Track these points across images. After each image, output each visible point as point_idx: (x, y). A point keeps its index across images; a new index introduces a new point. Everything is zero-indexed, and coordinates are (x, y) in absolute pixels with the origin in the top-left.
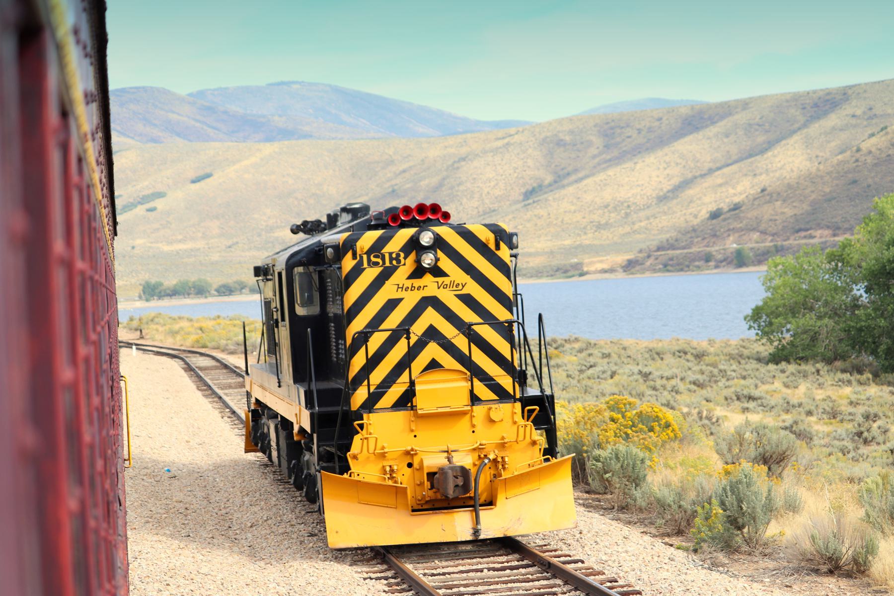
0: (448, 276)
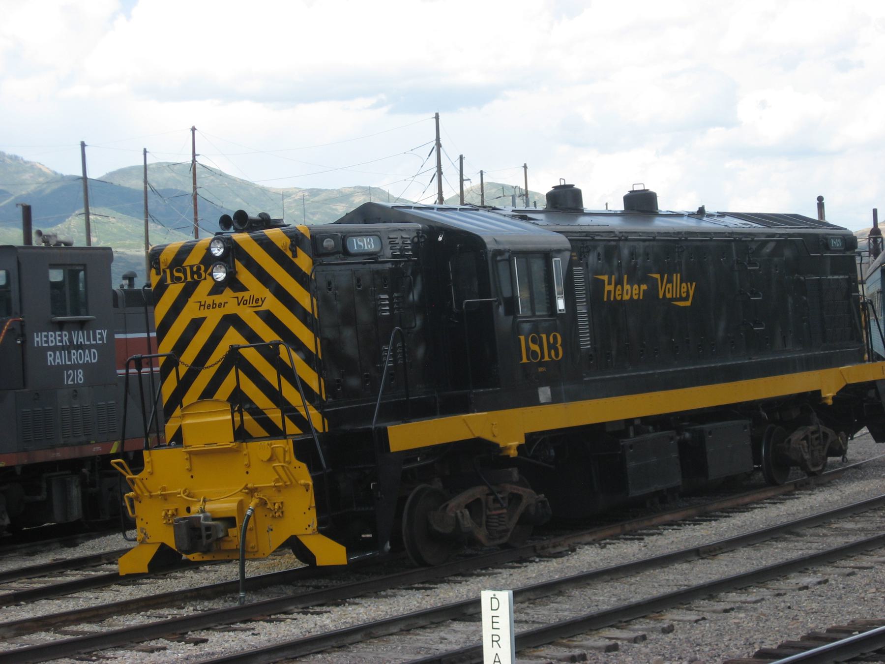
0: (248, 290)
